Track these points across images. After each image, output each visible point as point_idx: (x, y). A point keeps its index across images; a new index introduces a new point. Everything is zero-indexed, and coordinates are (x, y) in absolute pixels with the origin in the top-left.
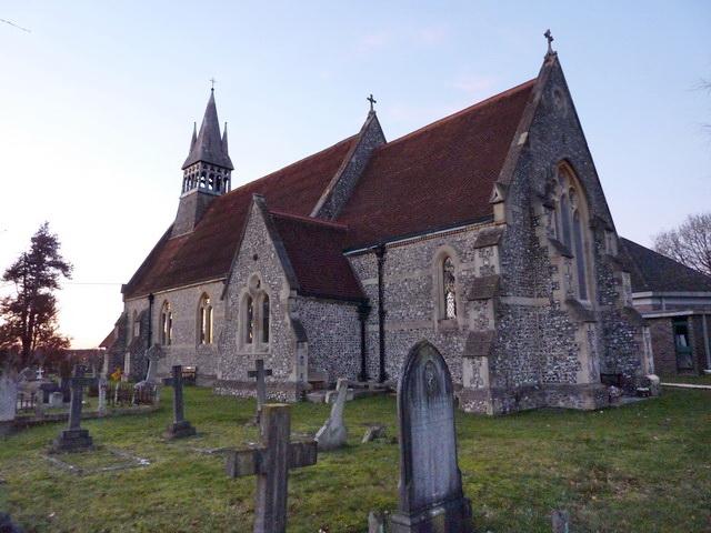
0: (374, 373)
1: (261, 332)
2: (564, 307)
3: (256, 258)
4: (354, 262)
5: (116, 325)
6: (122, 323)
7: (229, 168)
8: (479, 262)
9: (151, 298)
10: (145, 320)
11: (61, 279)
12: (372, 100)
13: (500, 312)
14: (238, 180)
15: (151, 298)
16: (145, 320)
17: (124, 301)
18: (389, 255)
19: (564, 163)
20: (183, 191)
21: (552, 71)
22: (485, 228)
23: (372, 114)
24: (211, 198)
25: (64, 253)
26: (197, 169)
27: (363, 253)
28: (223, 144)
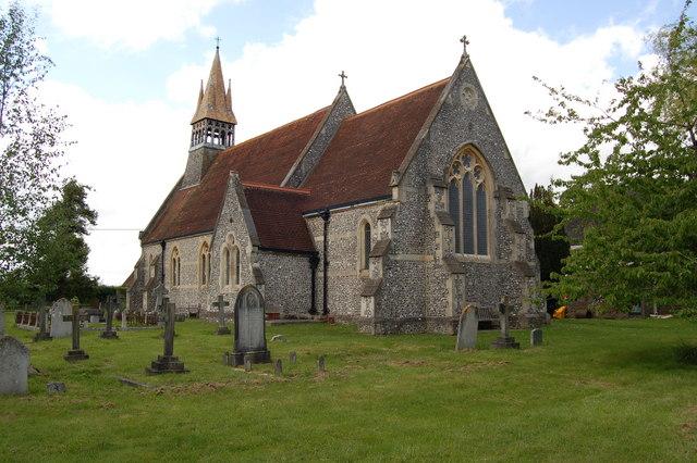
0: (320, 309)
1: (235, 276)
2: (441, 263)
3: (231, 221)
4: (310, 222)
5: (136, 267)
6: (140, 265)
7: (232, 125)
8: (380, 229)
9: (164, 245)
10: (159, 263)
11: (88, 226)
12: (343, 76)
13: (387, 266)
14: (241, 136)
15: (164, 245)
16: (159, 263)
17: (143, 245)
18: (332, 219)
19: (471, 147)
20: (192, 145)
21: (465, 72)
22: (388, 205)
23: (343, 89)
24: (216, 152)
25: (91, 201)
26: (204, 126)
27: (314, 216)
28: (227, 100)
